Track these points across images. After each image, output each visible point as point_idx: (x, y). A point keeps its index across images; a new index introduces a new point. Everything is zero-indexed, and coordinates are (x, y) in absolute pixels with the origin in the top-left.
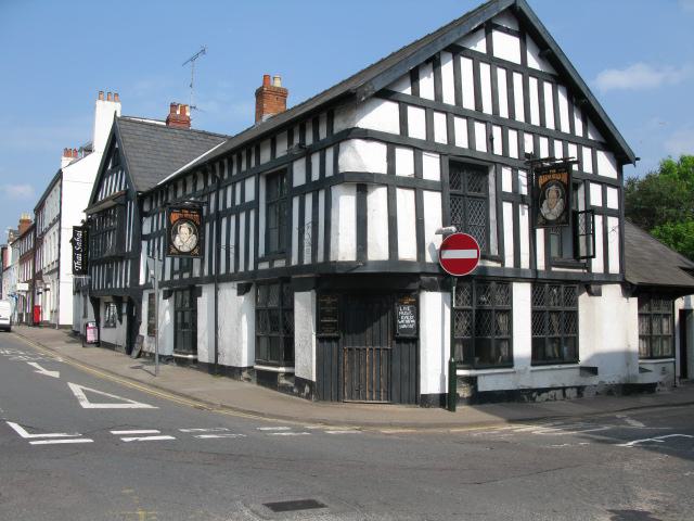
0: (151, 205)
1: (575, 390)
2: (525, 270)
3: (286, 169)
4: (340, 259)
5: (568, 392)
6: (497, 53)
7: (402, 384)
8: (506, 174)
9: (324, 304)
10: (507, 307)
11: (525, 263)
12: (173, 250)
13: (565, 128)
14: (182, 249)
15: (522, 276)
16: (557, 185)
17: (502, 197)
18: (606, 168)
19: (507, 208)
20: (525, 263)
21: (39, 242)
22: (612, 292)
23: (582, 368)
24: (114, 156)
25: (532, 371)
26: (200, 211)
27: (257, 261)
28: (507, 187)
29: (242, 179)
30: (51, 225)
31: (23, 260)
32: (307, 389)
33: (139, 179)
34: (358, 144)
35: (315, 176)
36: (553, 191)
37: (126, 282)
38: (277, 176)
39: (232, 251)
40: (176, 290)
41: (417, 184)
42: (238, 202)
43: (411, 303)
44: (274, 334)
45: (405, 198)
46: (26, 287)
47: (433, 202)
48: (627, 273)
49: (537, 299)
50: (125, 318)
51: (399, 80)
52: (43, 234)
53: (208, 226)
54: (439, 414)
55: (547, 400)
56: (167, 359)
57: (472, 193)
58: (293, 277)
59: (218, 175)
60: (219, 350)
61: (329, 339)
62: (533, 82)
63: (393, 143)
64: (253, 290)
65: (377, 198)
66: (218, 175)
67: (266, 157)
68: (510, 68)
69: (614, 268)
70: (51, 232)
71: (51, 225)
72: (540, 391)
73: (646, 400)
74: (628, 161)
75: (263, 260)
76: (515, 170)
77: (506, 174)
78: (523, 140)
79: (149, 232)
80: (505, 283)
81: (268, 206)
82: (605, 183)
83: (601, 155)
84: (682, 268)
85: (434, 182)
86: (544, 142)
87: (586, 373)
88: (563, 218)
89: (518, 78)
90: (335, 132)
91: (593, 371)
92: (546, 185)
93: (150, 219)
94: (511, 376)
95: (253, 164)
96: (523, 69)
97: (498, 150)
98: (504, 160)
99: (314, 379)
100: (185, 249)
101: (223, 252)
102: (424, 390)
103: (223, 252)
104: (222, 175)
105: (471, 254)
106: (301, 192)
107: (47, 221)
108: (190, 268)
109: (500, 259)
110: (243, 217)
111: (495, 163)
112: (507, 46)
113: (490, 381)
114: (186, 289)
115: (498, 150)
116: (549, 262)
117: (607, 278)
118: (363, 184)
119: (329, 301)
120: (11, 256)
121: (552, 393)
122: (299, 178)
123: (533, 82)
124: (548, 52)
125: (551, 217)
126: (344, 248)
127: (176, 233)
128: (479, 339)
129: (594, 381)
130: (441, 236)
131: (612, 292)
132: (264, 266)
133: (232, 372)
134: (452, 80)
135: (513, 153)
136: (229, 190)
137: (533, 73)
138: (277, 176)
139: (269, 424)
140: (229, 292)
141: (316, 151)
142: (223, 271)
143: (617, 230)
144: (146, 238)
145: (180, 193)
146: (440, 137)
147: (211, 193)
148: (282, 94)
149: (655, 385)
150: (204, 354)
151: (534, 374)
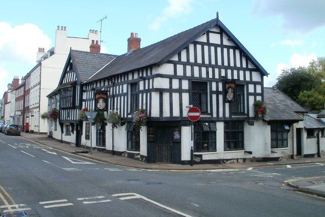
7: (175, 157)
8: (214, 84)
11: (221, 115)
12: (97, 109)
13: (238, 65)
19: (214, 96)
20: (221, 115)
21: (27, 92)
24: (70, 66)
26: (107, 94)
27: (128, 114)
28: (214, 89)
30: (34, 86)
31: (17, 100)
32: (144, 159)
33: (81, 77)
35: (147, 88)
37: (76, 117)
38: (134, 85)
41: (180, 91)
44: (133, 141)
45: (176, 96)
46: (19, 113)
47: (186, 97)
49: (225, 128)
50: (75, 132)
51: (172, 54)
53: (109, 99)
56: (94, 148)
61: (151, 142)
62: (225, 50)
63: (171, 78)
64: (126, 124)
65: (166, 96)
66: (113, 81)
67: (130, 78)
68: (216, 46)
70: (36, 88)
71: (34, 86)
72: (227, 160)
73: (68, 145)
74: (265, 75)
75: (130, 114)
76: (217, 83)
77: (214, 84)
80: (213, 122)
81: (131, 95)
82: (255, 84)
83: (254, 74)
84: (296, 112)
85: (186, 90)
86: (229, 71)
91: (250, 153)
94: (216, 155)
96: (222, 46)
98: (214, 79)
102: (183, 159)
104: (115, 80)
105: (197, 114)
106: (142, 92)
107: (32, 85)
109: (211, 114)
110: (122, 98)
112: (215, 38)
113: (207, 156)
115: (211, 76)
116: (231, 113)
118: (161, 92)
121: (232, 161)
122: (141, 88)
123: (225, 50)
124: (231, 38)
125: (230, 99)
126: (155, 113)
127: (98, 102)
128: (204, 140)
129: (251, 156)
133: (120, 154)
134: (194, 53)
135: (217, 76)
136: (118, 87)
137: (226, 46)
138: (134, 85)
145: (98, 86)
146: (189, 74)
148: (139, 40)
149: (279, 158)
150: (109, 146)
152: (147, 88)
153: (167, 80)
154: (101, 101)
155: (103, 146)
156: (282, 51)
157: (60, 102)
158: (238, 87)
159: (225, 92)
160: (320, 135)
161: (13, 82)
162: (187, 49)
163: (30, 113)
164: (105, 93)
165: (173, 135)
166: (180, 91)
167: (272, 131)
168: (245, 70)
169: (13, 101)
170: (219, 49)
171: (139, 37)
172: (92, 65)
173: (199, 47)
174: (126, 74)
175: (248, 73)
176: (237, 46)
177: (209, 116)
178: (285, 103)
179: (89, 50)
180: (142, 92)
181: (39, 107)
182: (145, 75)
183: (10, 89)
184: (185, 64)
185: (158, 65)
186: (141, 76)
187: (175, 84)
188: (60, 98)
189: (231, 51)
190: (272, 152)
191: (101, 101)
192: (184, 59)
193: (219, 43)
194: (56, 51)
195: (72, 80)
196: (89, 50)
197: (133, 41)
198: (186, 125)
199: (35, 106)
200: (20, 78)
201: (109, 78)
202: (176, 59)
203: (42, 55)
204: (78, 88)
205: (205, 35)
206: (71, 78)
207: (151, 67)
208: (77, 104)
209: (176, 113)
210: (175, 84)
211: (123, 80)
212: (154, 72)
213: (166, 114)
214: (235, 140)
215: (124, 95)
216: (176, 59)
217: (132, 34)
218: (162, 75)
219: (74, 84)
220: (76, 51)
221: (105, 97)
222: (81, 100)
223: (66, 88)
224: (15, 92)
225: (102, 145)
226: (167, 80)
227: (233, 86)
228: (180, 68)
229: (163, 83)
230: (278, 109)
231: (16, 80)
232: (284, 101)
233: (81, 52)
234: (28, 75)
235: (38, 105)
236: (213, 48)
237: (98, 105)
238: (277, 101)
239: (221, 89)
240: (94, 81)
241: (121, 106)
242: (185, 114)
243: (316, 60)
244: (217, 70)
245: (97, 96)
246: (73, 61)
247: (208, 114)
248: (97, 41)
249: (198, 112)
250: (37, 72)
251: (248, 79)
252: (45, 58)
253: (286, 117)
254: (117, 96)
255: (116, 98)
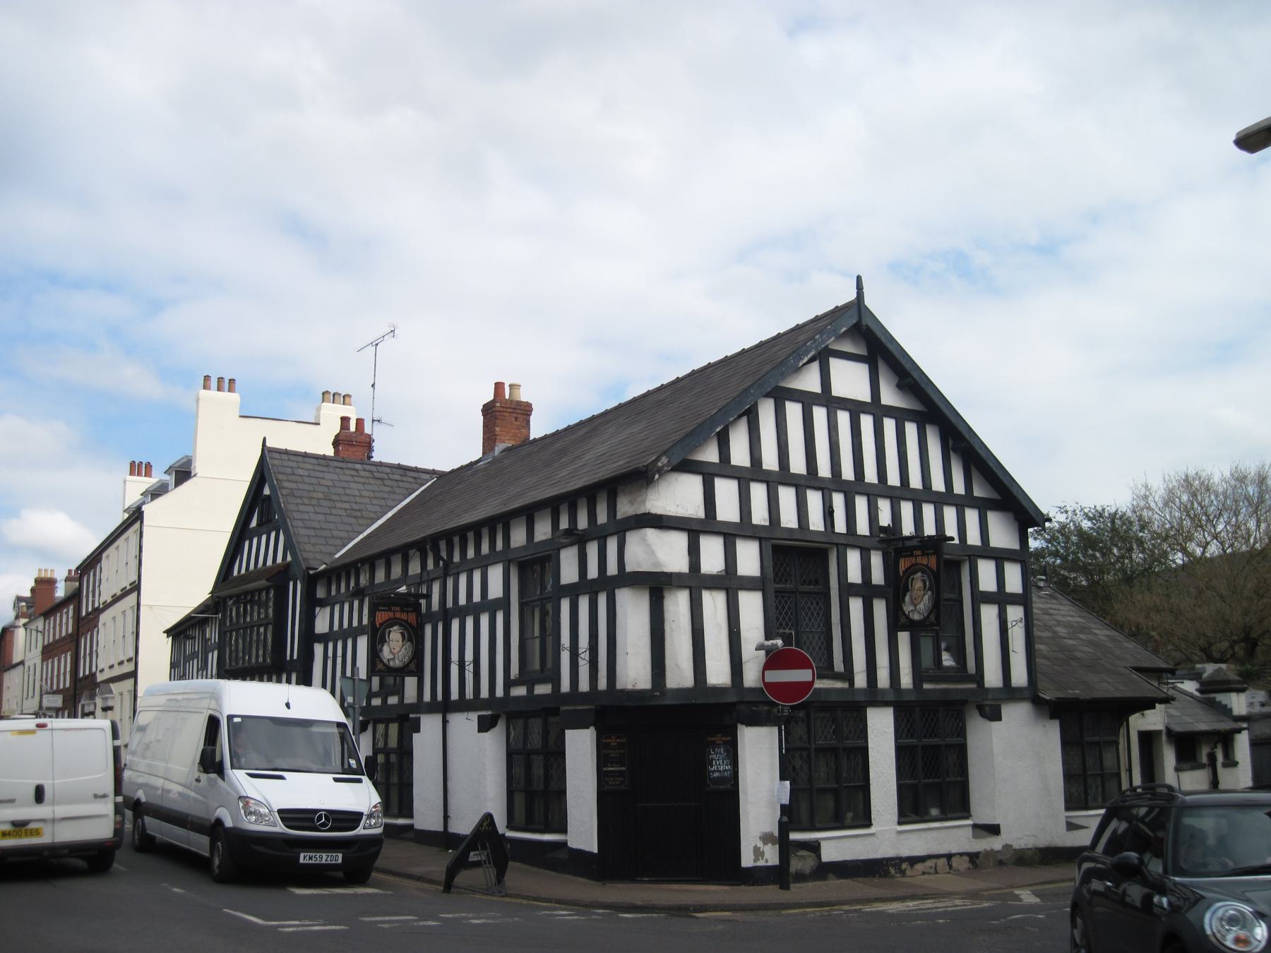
0: (329, 591)
1: (967, 858)
2: (883, 690)
3: (549, 556)
4: (630, 687)
5: (955, 861)
6: (838, 390)
8: (853, 559)
9: (607, 746)
10: (859, 743)
11: (883, 679)
12: (380, 666)
13: (938, 484)
14: (391, 663)
15: (880, 698)
16: (923, 572)
17: (848, 590)
18: (1002, 535)
19: (856, 606)
20: (883, 679)
21: (87, 623)
22: (1016, 715)
23: (975, 826)
24: (262, 506)
25: (900, 832)
27: (508, 684)
28: (854, 575)
29: (484, 564)
30: (116, 599)
31: (49, 652)
33: (308, 547)
34: (651, 533)
35: (593, 573)
36: (918, 582)
38: (534, 568)
39: (469, 669)
40: (376, 722)
42: (477, 597)
43: (725, 743)
44: (535, 786)
45: (714, 603)
47: (751, 606)
48: (1040, 685)
51: (696, 437)
52: (98, 611)
54: (770, 893)
55: (924, 873)
57: (806, 588)
58: (563, 708)
59: (444, 554)
60: (451, 813)
62: (889, 425)
63: (695, 530)
65: (678, 605)
66: (444, 554)
67: (518, 537)
69: (1019, 676)
71: (116, 599)
72: (913, 861)
75: (517, 683)
77: (853, 559)
78: (877, 508)
79: (326, 630)
82: (1000, 557)
83: (993, 519)
84: (1139, 670)
86: (907, 509)
87: (983, 833)
88: (932, 618)
89: (867, 422)
90: (619, 516)
91: (994, 830)
92: (911, 571)
93: (328, 609)
95: (499, 545)
96: (877, 409)
97: (840, 526)
99: (1102, 811)
100: (397, 663)
101: (454, 670)
102: (747, 860)
103: (454, 670)
104: (450, 554)
105: (803, 675)
106: (573, 592)
107: (107, 590)
108: (400, 691)
109: (848, 675)
110: (485, 620)
111: (837, 545)
112: (850, 379)
113: (837, 846)
114: (393, 721)
115: (840, 526)
117: (1009, 692)
118: (656, 585)
119: (613, 741)
120: (24, 645)
121: (930, 863)
123: (889, 425)
124: (910, 379)
125: (916, 617)
126: (634, 671)
127: (383, 641)
128: (828, 786)
129: (995, 844)
130: (763, 653)
131: (1016, 715)
132: (520, 691)
134: (779, 435)
135: (863, 528)
136: (463, 579)
137: (890, 411)
138: (534, 568)
139: (548, 909)
140: (464, 724)
141: (593, 539)
142: (455, 695)
143: (1022, 625)
144: (324, 639)
145: (380, 576)
146: (760, 516)
147: (432, 580)
148: (525, 410)
151: (903, 837)
152: (593, 573)
153: (679, 541)
154: (395, 635)
155: (401, 815)
156: (1095, 420)
157: (221, 647)
158: (941, 563)
159: (895, 590)
160: (1220, 758)
161: (33, 590)
162: (752, 417)
163: (99, 701)
164: (410, 603)
165: (704, 763)
166: (729, 583)
167: (1065, 743)
168: (961, 504)
169: (34, 658)
170: (867, 422)
171: (524, 397)
172: (347, 506)
173: (794, 411)
174: (502, 522)
175: (972, 516)
176: (930, 410)
177: (839, 685)
178: (1091, 637)
179: (330, 452)
180: (573, 592)
181: (133, 675)
182: (583, 523)
183: (24, 616)
184: (745, 478)
185: (641, 478)
186: (564, 524)
187: (712, 556)
188: (222, 634)
189: (911, 430)
190: (1071, 826)
191: (395, 635)
192: (740, 455)
193: (864, 395)
194: (198, 467)
195: (269, 563)
196: (330, 452)
197: (503, 413)
198: (755, 721)
199: (118, 671)
200: (60, 574)
201: (426, 546)
202: (710, 454)
203: (145, 483)
204: (296, 592)
205: (815, 366)
206: (266, 552)
207: (613, 487)
208: (293, 650)
209: (718, 673)
210: (712, 556)
211: (485, 549)
212: (625, 508)
213: (680, 674)
214: (936, 781)
215: (491, 607)
216: (710, 454)
217: (499, 387)
218: (660, 517)
219: (279, 577)
220: (286, 452)
221: (412, 618)
222: (309, 636)
223: (246, 593)
224: (40, 624)
225: (395, 810)
226: (679, 541)
227: (932, 562)
228: (726, 490)
229: (669, 552)
230: (1074, 659)
231: (44, 584)
232: (1083, 629)
233: (305, 455)
234: (92, 562)
235: (128, 668)
236: (843, 418)
237: (386, 649)
238: (1061, 630)
239: (878, 577)
240: (363, 561)
241: (483, 650)
242: (751, 677)
243: (1172, 474)
244: (861, 504)
245: (381, 617)
246: (272, 488)
247: (837, 677)
248: (360, 422)
249: (805, 665)
250: (127, 543)
251: (973, 538)
252: (157, 492)
253: (1107, 687)
254: (462, 613)
255: (455, 625)
